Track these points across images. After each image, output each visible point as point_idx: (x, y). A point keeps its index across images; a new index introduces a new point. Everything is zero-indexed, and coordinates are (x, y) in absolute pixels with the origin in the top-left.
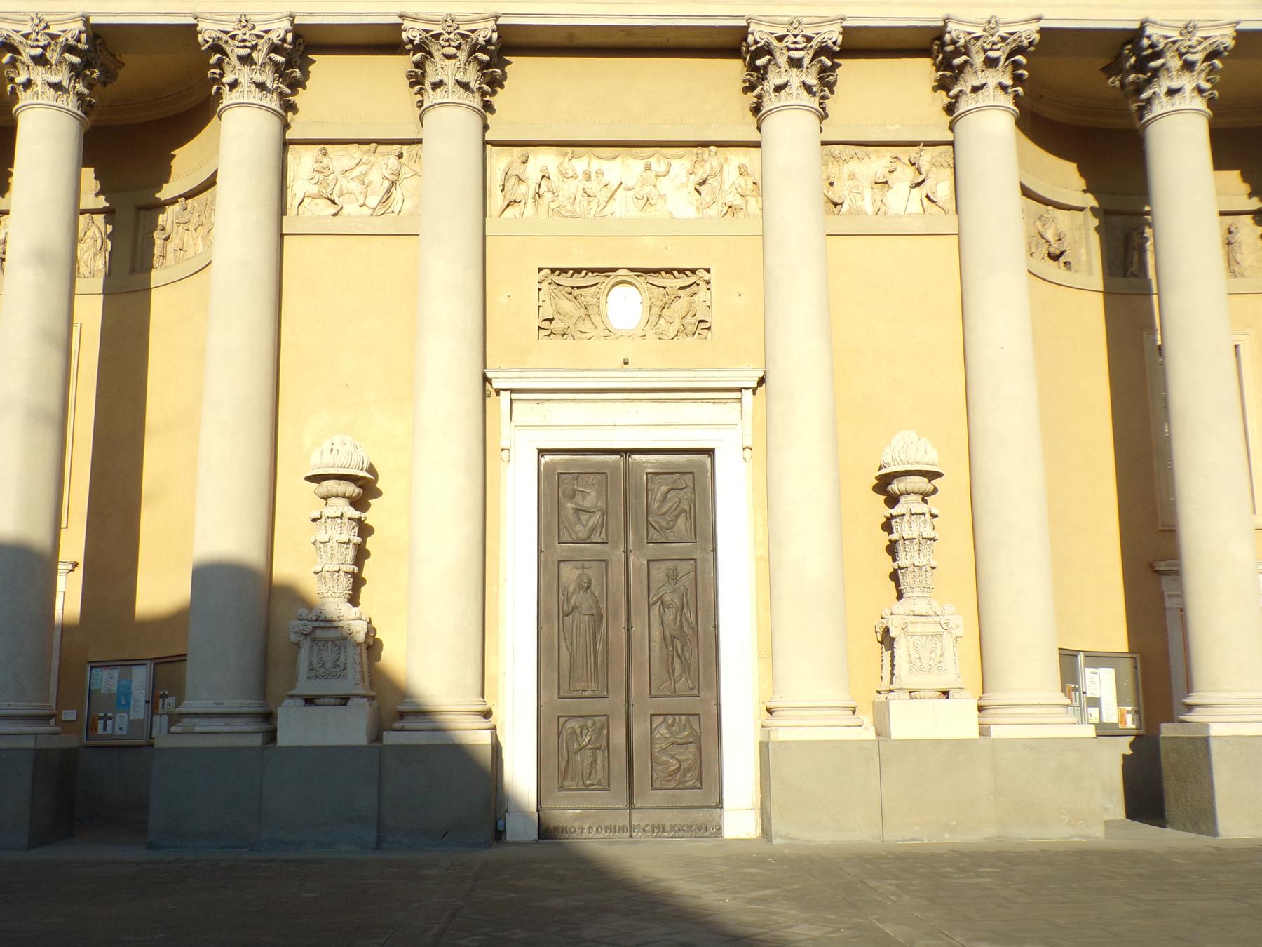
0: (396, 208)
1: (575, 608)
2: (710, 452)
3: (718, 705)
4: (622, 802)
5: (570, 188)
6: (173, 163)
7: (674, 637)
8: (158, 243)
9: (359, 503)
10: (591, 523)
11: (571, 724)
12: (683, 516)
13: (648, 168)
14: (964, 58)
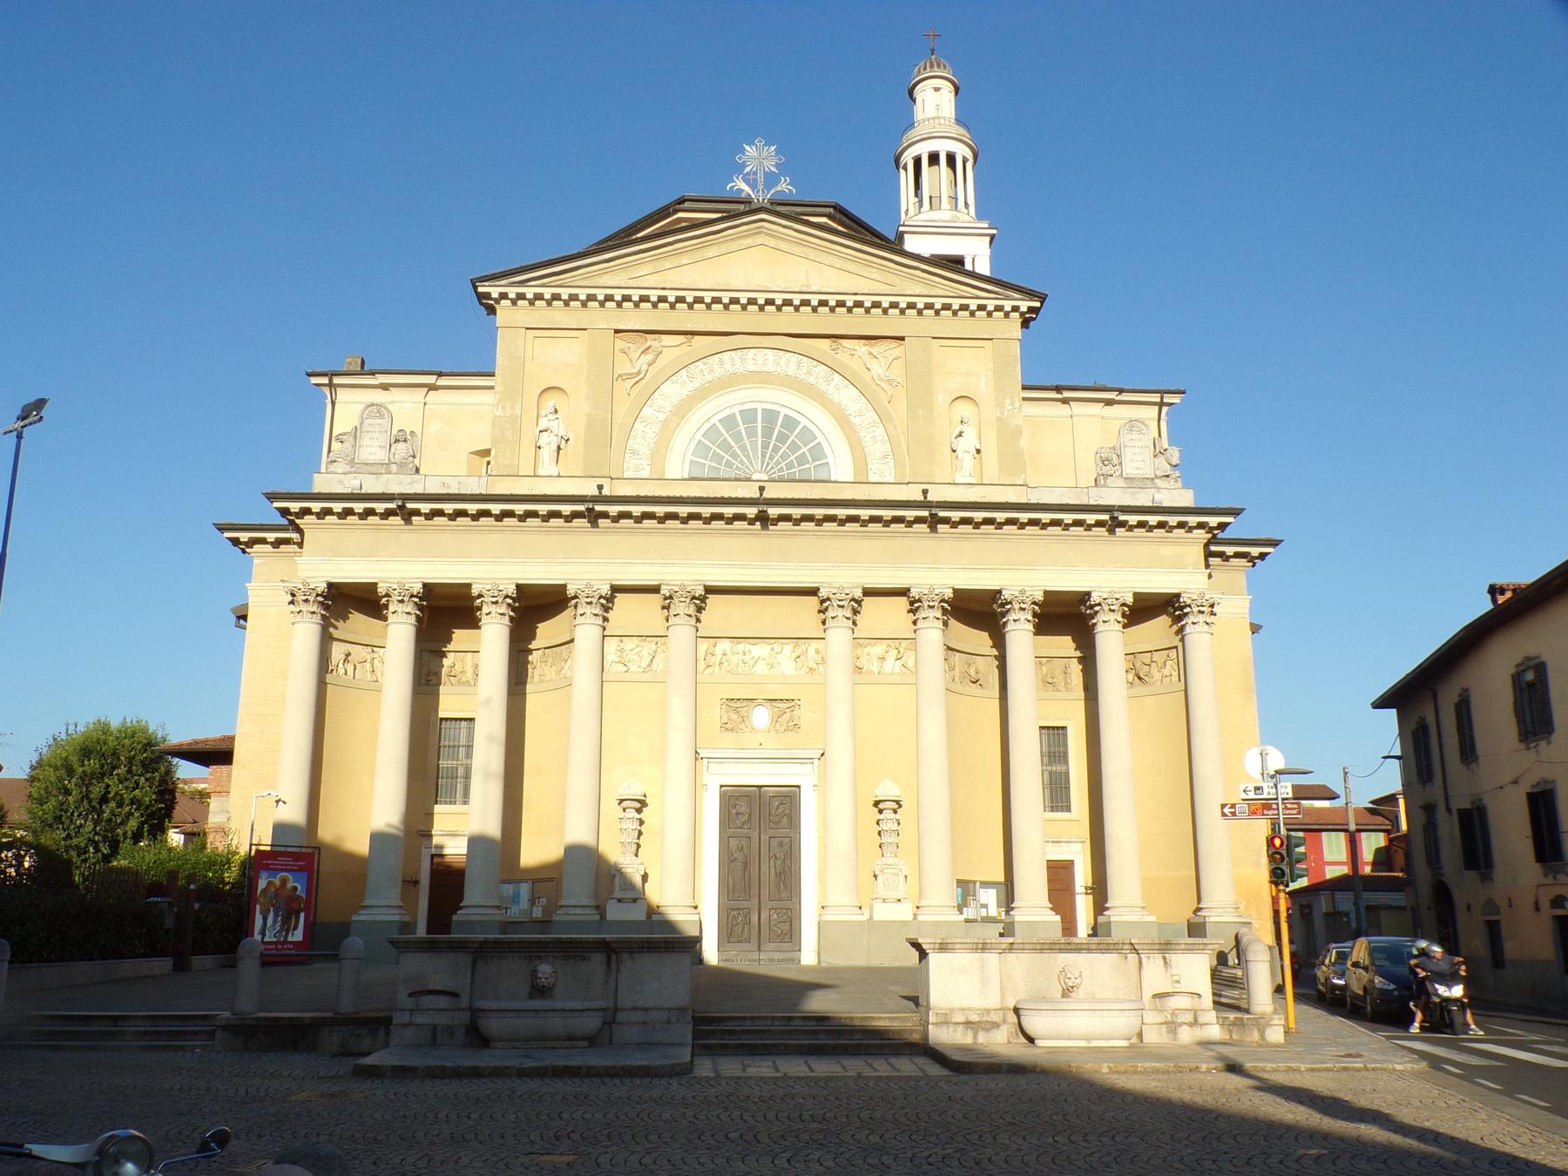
0: (655, 668)
1: (735, 859)
2: (799, 787)
3: (800, 904)
4: (756, 948)
5: (735, 659)
6: (538, 630)
7: (780, 873)
8: (530, 670)
9: (639, 811)
10: (744, 819)
11: (733, 913)
12: (785, 817)
13: (772, 649)
14: (919, 604)
